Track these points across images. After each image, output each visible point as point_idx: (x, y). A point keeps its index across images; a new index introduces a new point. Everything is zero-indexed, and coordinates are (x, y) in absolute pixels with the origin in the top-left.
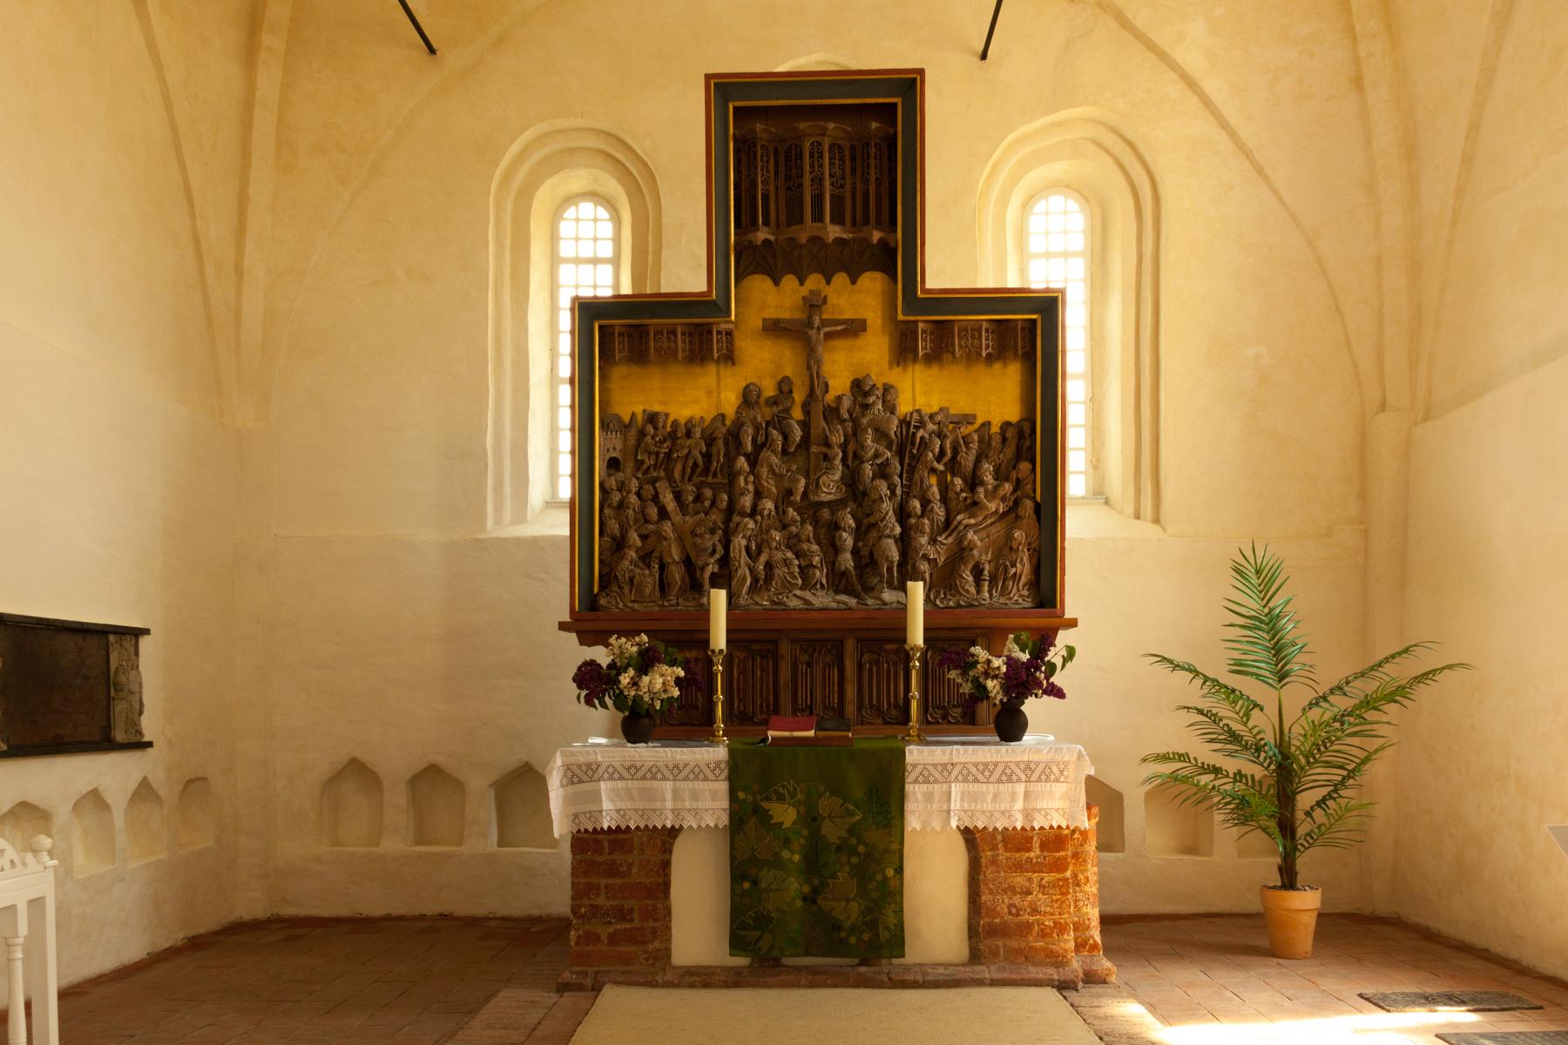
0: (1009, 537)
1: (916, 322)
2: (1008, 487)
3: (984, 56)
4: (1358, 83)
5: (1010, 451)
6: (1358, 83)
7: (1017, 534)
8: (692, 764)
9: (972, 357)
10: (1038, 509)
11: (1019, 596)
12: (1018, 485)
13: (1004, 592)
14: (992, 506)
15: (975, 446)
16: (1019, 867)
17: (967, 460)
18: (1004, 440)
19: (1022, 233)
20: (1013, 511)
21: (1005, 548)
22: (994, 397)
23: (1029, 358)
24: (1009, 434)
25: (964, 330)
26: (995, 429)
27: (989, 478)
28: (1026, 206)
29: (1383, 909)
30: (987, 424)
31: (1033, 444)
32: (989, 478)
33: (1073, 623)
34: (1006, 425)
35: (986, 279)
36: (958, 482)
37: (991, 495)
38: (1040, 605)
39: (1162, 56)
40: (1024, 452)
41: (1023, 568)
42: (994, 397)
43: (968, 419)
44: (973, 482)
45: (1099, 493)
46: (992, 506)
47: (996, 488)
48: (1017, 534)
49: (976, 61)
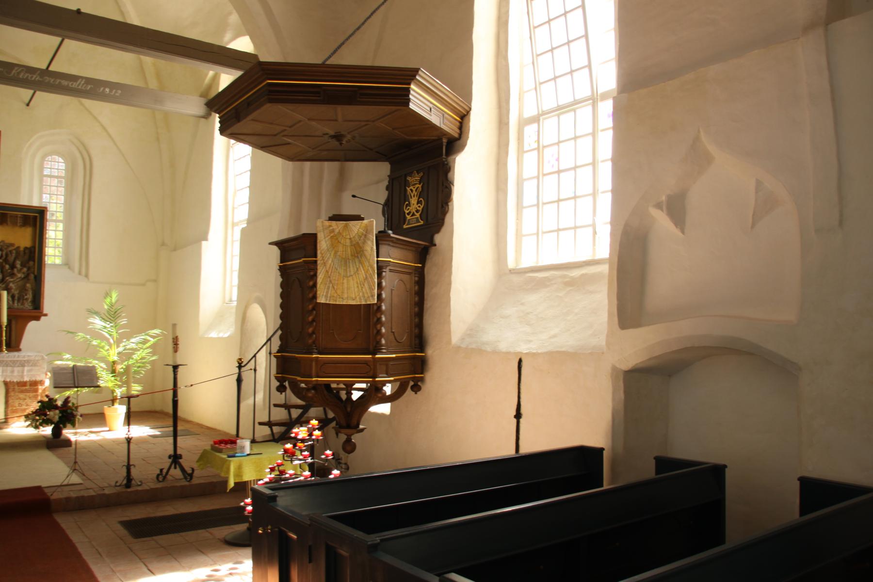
0: (25, 286)
1: (34, 261)
2: (25, 270)
3: (28, 105)
4: (158, 139)
5: (26, 257)
6: (158, 139)
7: (28, 285)
8: (16, 246)
9: (14, 224)
10: (35, 277)
11: (28, 305)
12: (29, 269)
13: (23, 304)
14: (19, 275)
15: (14, 255)
16: (22, 392)
17: (11, 259)
18: (25, 253)
19: (41, 168)
20: (27, 277)
21: (23, 290)
22: (22, 238)
23: (35, 226)
24: (27, 251)
25: (11, 216)
26: (22, 249)
27: (18, 266)
28: (43, 159)
29: (158, 409)
30: (19, 247)
31: (34, 255)
32: (18, 266)
33: (46, 315)
34: (26, 248)
35: (24, 201)
36: (7, 267)
37: (19, 271)
38: (35, 309)
39: (95, 118)
40: (32, 258)
41: (29, 296)
42: (22, 238)
43: (12, 245)
44: (13, 267)
45: (79, 262)
46: (19, 275)
47: (21, 269)
48: (28, 285)
49: (25, 106)
